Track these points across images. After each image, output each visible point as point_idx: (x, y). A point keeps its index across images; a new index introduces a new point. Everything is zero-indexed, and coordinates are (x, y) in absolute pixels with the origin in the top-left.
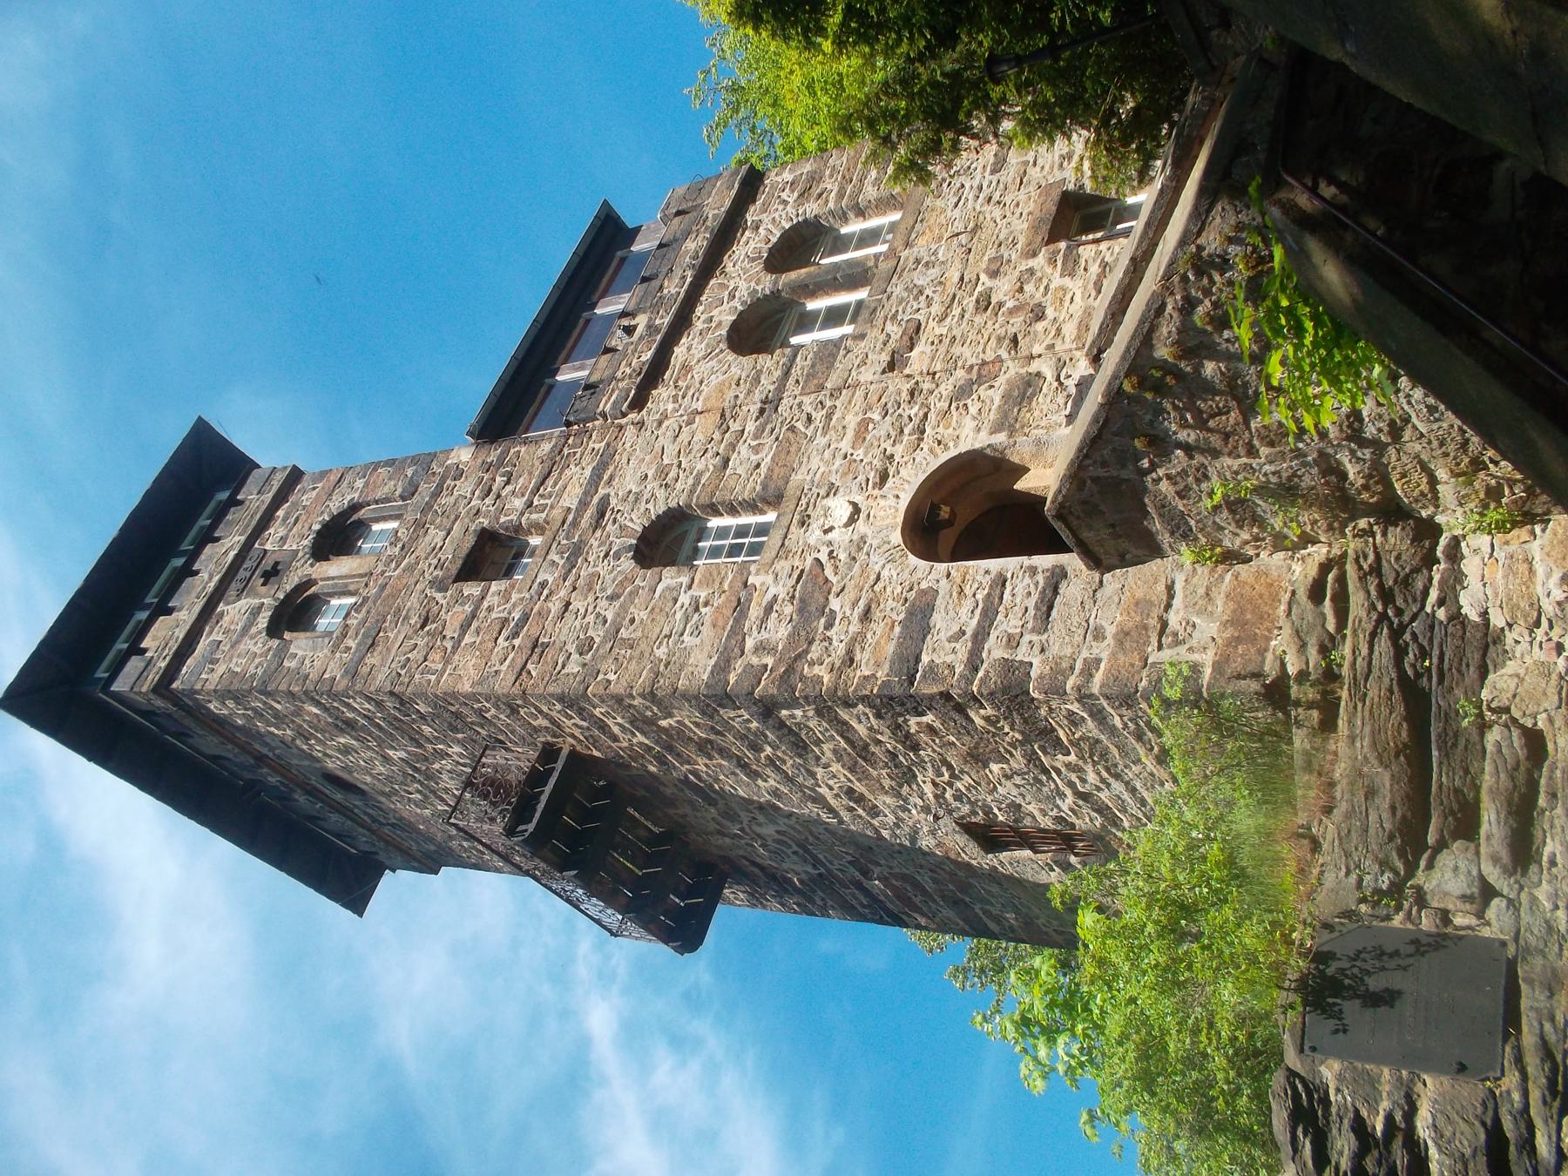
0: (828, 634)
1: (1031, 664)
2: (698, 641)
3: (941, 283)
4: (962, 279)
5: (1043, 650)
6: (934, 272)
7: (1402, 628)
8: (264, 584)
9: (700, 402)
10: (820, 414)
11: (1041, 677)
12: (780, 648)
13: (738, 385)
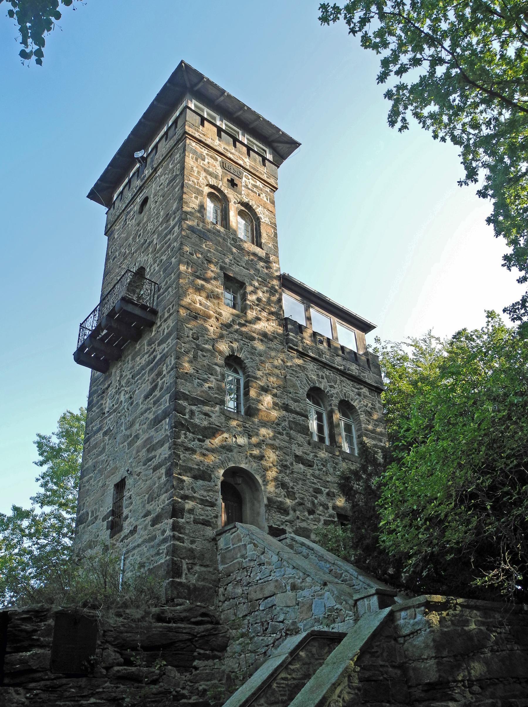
0: (196, 440)
1: (183, 518)
2: (196, 386)
3: (327, 473)
4: (328, 482)
5: (187, 522)
6: (331, 470)
7: (192, 642)
8: (228, 180)
9: (289, 377)
10: (280, 429)
11: (178, 522)
12: (192, 421)
13: (295, 393)
